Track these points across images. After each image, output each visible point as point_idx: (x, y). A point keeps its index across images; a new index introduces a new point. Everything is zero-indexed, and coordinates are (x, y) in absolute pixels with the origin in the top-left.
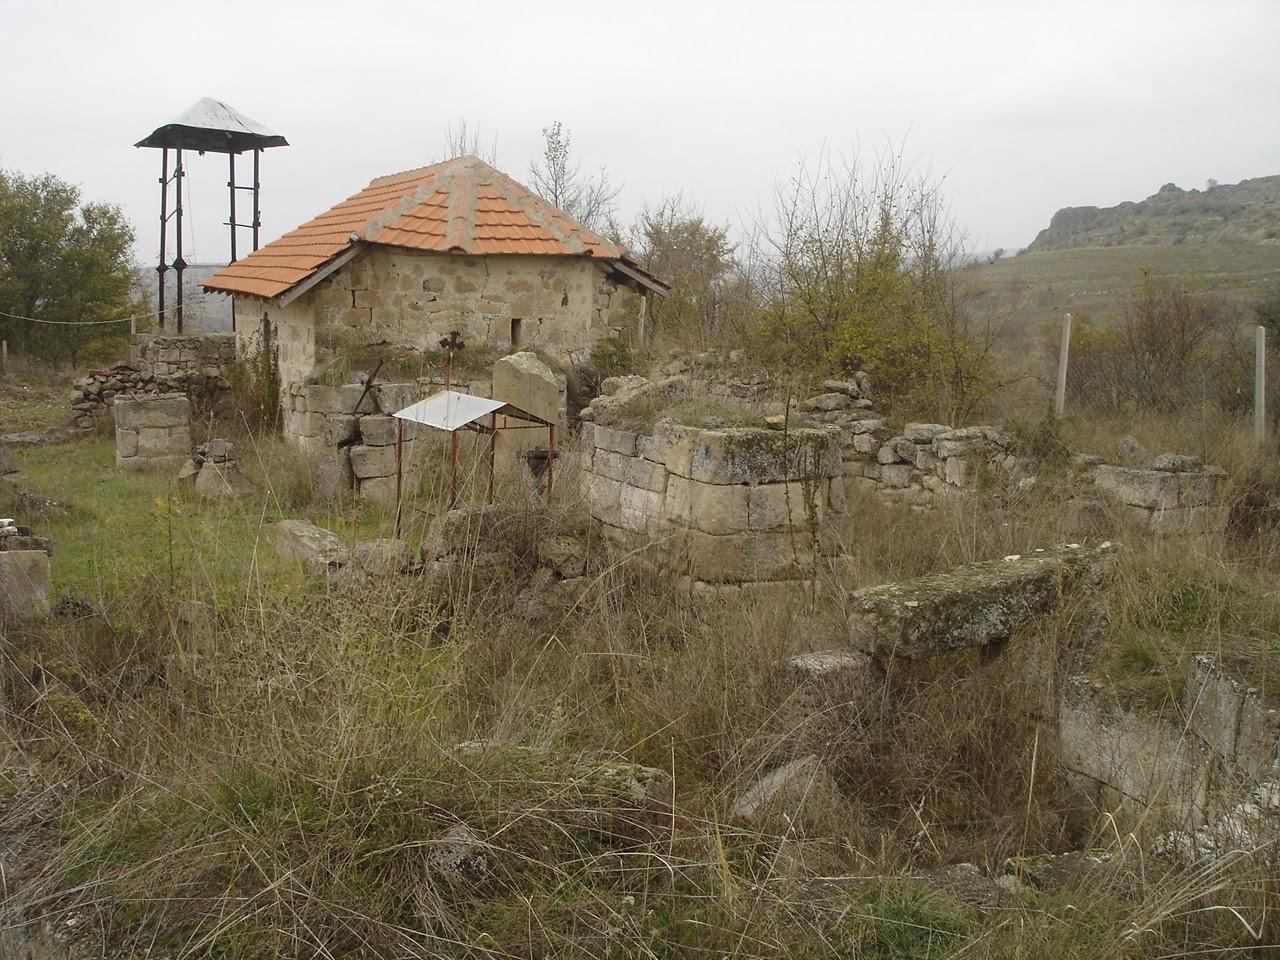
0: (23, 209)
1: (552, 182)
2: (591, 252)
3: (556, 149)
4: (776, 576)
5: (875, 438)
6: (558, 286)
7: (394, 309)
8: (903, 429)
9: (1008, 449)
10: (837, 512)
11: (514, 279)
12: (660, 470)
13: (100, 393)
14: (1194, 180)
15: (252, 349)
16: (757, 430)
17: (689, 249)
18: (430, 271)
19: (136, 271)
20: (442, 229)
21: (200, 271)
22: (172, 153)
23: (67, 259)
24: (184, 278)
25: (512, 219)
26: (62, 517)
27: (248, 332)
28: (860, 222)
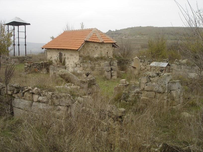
14: (113, 29)
18: (96, 45)
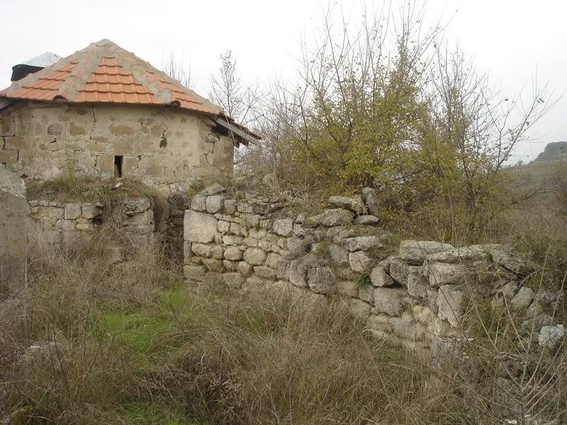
2: (179, 104)
5: (369, 256)
6: (156, 131)
9: (521, 277)
11: (117, 124)
25: (125, 80)
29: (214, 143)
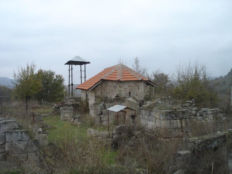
0: (45, 76)
1: (136, 68)
2: (143, 79)
3: (137, 62)
4: (176, 137)
6: (137, 86)
7: (109, 91)
8: (201, 109)
9: (221, 113)
10: (188, 125)
11: (129, 85)
12: (154, 118)
13: (58, 107)
15: (84, 99)
16: (171, 110)
17: (162, 79)
18: (114, 84)
19: (65, 86)
20: (117, 76)
21: (76, 85)
22: (71, 65)
23: (53, 84)
24: (73, 87)
25: (129, 74)
26: (51, 128)
27: (83, 96)
28: (191, 72)
29: (147, 87)
